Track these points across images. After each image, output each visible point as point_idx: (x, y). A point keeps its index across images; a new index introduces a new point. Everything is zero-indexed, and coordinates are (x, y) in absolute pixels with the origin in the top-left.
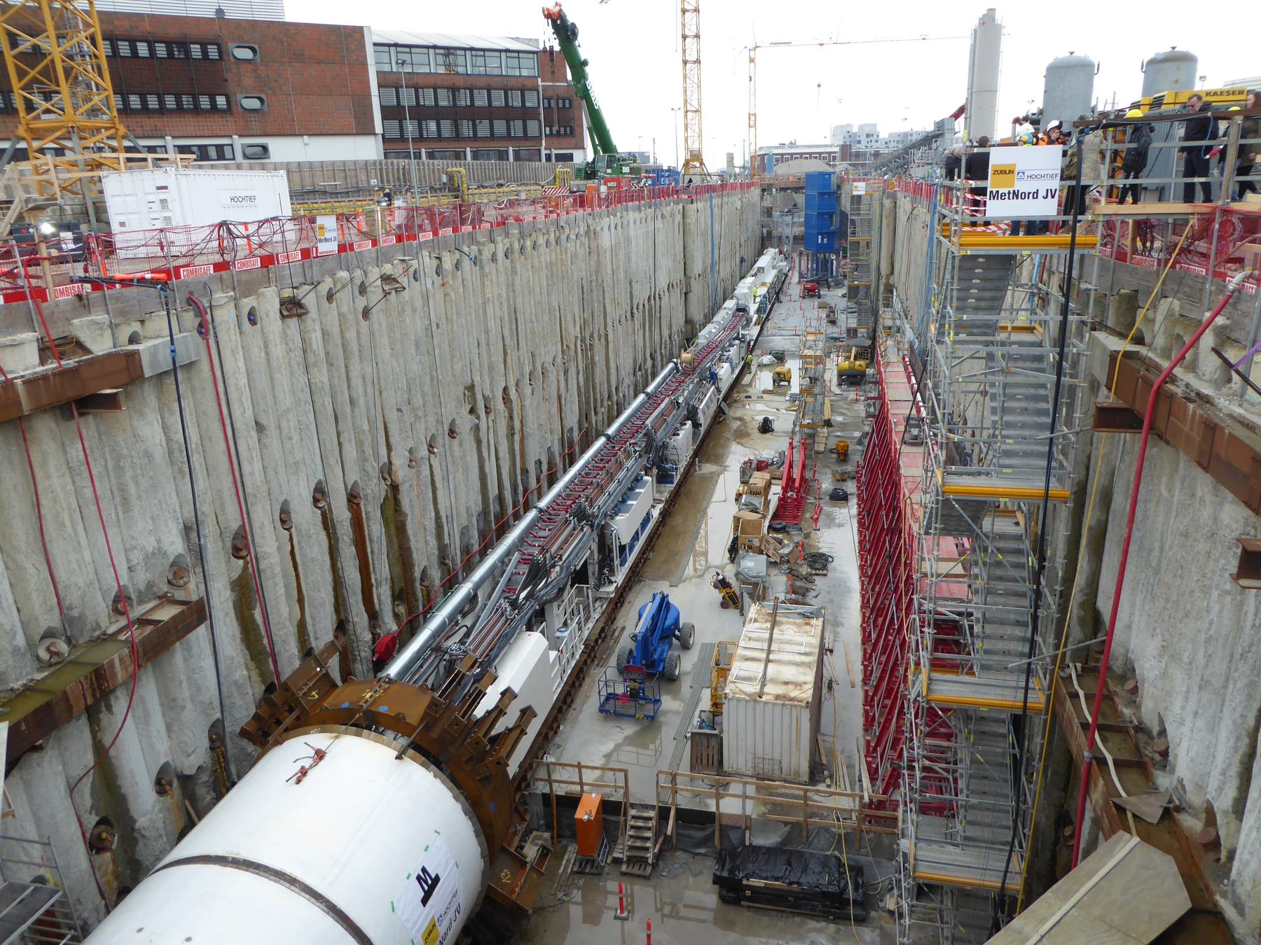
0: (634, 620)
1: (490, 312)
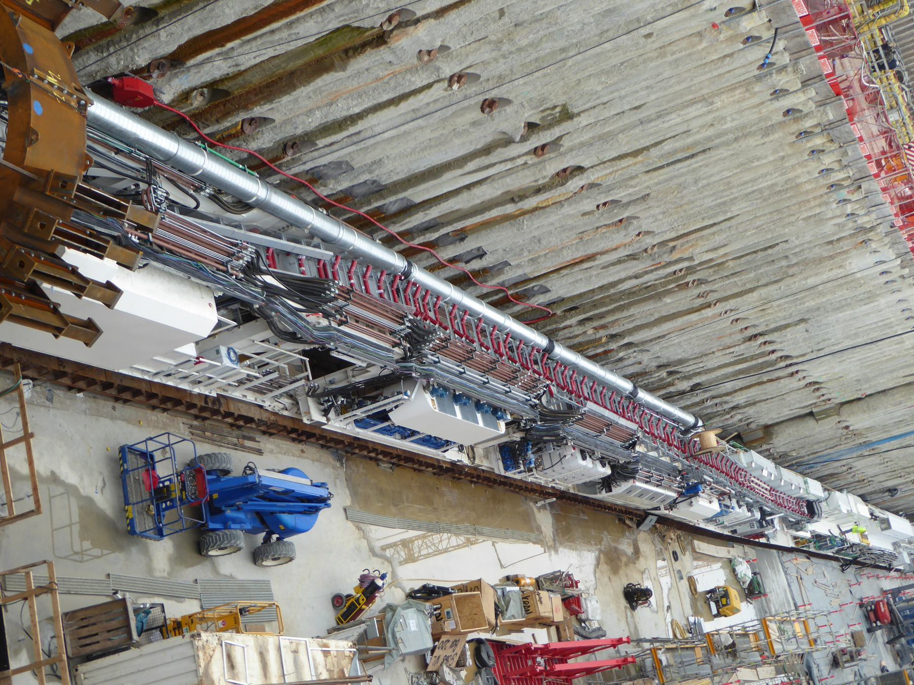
0: (276, 465)
1: (693, 111)
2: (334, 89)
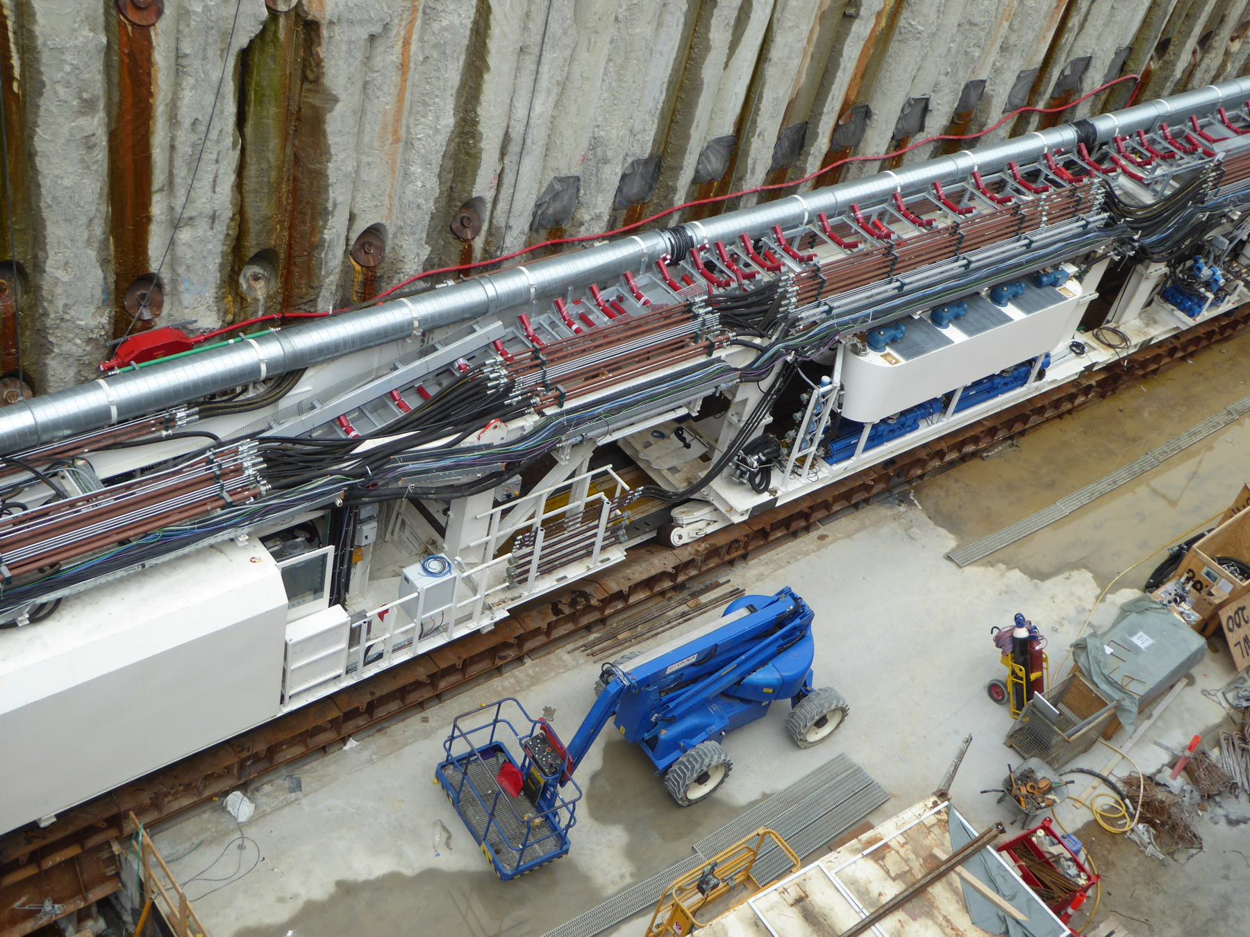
2: (377, 128)
